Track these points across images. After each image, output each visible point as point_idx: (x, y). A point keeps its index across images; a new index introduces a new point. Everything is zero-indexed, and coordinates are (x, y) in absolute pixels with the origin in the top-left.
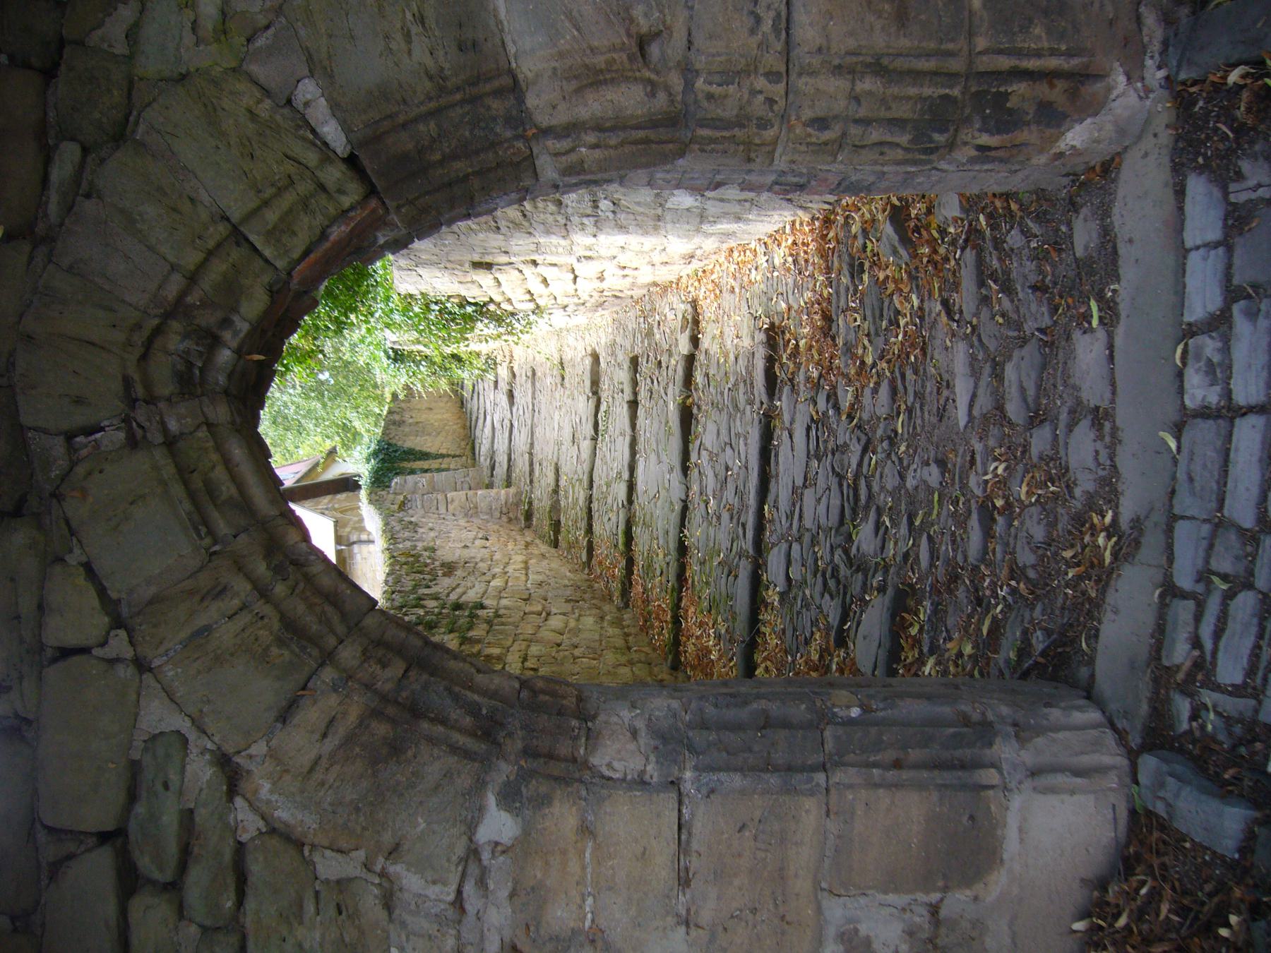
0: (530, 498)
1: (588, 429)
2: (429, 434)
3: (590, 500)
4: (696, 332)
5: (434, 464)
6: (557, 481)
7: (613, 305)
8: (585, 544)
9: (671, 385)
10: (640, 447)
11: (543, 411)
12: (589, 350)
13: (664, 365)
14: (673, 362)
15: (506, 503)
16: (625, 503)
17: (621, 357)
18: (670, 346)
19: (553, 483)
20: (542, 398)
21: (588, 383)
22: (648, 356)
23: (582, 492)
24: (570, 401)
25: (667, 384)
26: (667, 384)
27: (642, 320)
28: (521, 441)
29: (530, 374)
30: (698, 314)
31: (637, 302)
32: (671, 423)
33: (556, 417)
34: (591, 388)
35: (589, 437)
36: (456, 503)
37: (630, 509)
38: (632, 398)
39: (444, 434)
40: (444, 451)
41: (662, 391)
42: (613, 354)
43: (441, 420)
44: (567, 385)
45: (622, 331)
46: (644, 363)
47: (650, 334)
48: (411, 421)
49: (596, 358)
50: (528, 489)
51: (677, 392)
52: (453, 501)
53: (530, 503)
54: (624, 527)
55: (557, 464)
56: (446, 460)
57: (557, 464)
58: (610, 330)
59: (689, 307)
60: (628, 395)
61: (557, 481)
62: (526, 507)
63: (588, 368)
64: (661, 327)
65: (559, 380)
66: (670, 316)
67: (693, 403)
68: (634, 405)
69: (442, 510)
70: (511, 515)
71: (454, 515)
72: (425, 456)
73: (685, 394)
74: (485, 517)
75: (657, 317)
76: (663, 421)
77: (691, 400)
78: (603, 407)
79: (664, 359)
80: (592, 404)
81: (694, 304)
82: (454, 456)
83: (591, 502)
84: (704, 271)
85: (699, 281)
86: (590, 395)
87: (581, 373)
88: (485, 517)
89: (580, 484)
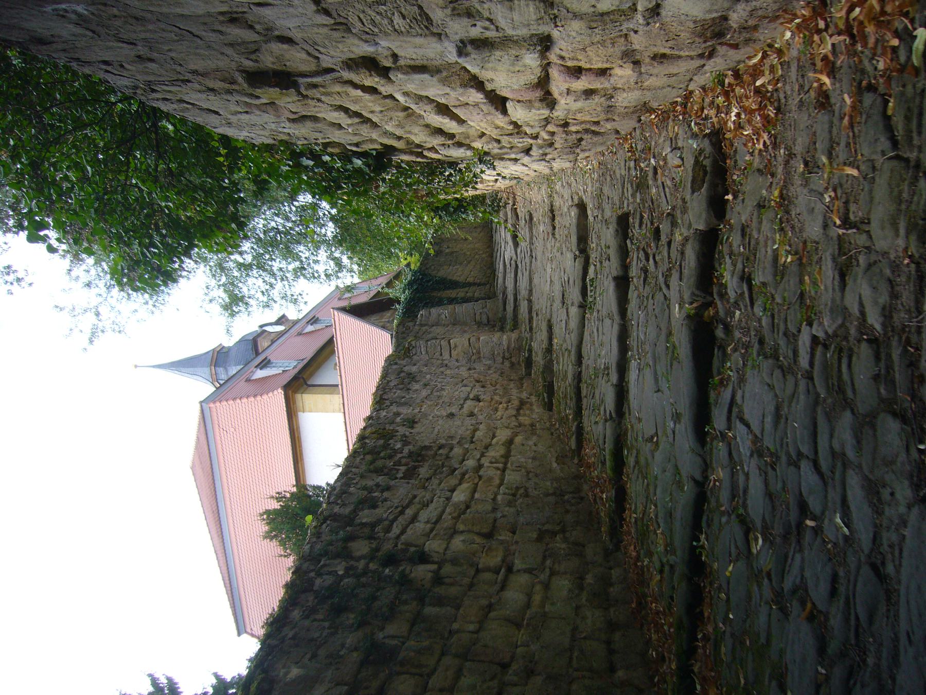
0: (530, 345)
1: (574, 294)
2: (461, 264)
3: (578, 377)
4: (720, 189)
5: (461, 293)
6: (550, 339)
7: (595, 144)
8: (574, 429)
9: (675, 275)
10: (632, 342)
11: (539, 258)
12: (576, 201)
13: (664, 239)
14: (678, 238)
15: (508, 348)
16: (614, 415)
17: (608, 213)
18: (673, 208)
19: (546, 342)
20: (539, 245)
21: (574, 239)
22: (642, 217)
23: (570, 367)
24: (558, 254)
25: (670, 270)
26: (670, 270)
27: (632, 164)
28: (523, 284)
29: (527, 218)
30: (724, 157)
31: (626, 139)
32: (674, 339)
33: (549, 270)
34: (578, 245)
35: (576, 304)
36: (459, 349)
37: (620, 423)
38: (621, 273)
39: (473, 263)
40: (471, 280)
41: (661, 279)
42: (600, 207)
43: (473, 249)
44: (557, 236)
45: (608, 178)
46: (637, 225)
47: (641, 186)
48: (447, 251)
49: (582, 207)
50: (528, 336)
51: (687, 296)
52: (456, 346)
53: (530, 351)
54: (611, 446)
55: (549, 321)
56: (473, 288)
57: (549, 321)
58: (595, 176)
59: (706, 144)
60: (591, 316)
61: (550, 339)
62: (527, 355)
63: (574, 221)
64: (659, 176)
65: (550, 229)
66: (673, 160)
67: (716, 318)
68: (622, 283)
69: (446, 355)
70: (513, 359)
71: (457, 361)
72: (454, 285)
73: (701, 300)
74: (488, 362)
75: (652, 161)
76: (664, 331)
77: (711, 311)
78: (591, 269)
79: (665, 227)
80: (579, 264)
81: (717, 137)
82: (479, 285)
83: (580, 381)
84: (737, 74)
85: (726, 94)
86: (577, 253)
87: (568, 225)
88: (488, 362)
89: (569, 355)
